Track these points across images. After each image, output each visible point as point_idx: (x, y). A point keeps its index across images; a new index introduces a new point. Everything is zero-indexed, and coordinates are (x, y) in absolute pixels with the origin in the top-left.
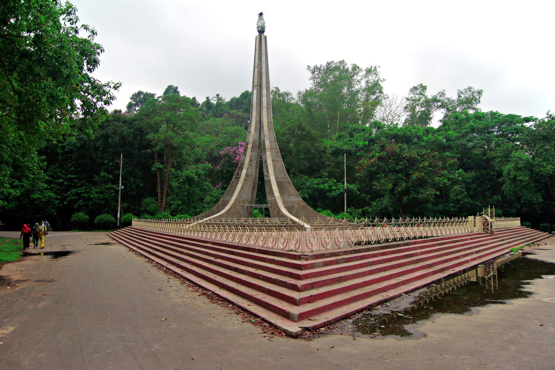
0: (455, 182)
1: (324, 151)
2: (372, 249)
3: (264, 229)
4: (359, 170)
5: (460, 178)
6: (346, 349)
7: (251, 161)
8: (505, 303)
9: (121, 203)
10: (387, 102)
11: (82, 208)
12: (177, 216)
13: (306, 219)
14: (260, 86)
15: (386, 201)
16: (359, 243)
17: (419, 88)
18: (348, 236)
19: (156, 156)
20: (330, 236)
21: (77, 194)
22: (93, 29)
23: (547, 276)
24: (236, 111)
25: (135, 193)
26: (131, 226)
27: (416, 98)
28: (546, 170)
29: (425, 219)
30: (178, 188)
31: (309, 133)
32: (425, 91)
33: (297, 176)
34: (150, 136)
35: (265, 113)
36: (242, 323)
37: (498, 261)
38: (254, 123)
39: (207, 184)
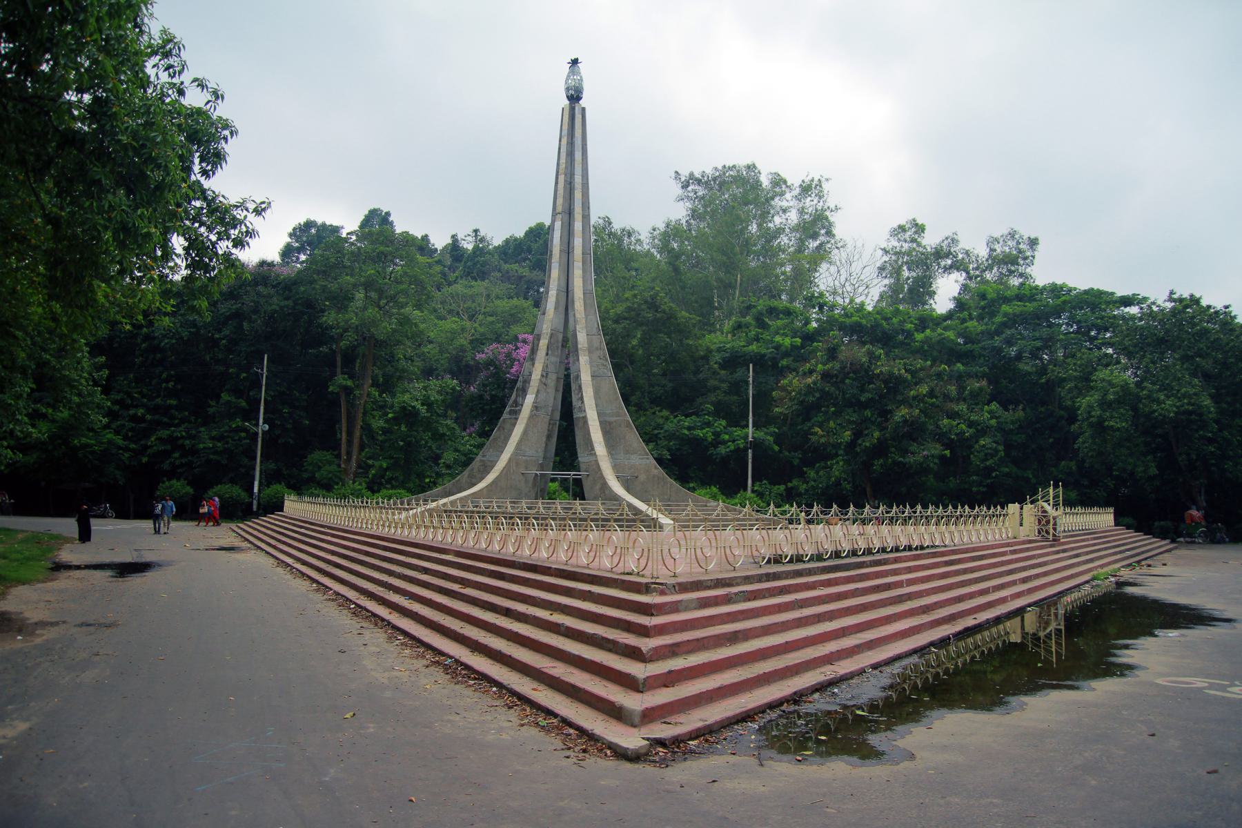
0: (982, 431)
1: (706, 358)
2: (804, 573)
3: (570, 526)
4: (782, 399)
5: (993, 422)
6: (743, 786)
7: (545, 375)
8: (1077, 688)
9: (261, 462)
10: (843, 254)
11: (179, 471)
12: (381, 493)
13: (664, 505)
14: (570, 213)
15: (838, 468)
16: (777, 560)
17: (909, 228)
18: (753, 544)
19: (339, 359)
20: (714, 544)
21: (172, 440)
22: (216, 87)
23: (1165, 631)
24: (515, 266)
25: (292, 442)
26: (282, 511)
27: (903, 250)
28: (1162, 409)
29: (919, 508)
30: (385, 431)
31: (671, 316)
32: (922, 234)
33: (646, 410)
34: (330, 318)
35: (577, 273)
36: (519, 728)
37: (1068, 598)
38: (553, 293)
39: (448, 423)
